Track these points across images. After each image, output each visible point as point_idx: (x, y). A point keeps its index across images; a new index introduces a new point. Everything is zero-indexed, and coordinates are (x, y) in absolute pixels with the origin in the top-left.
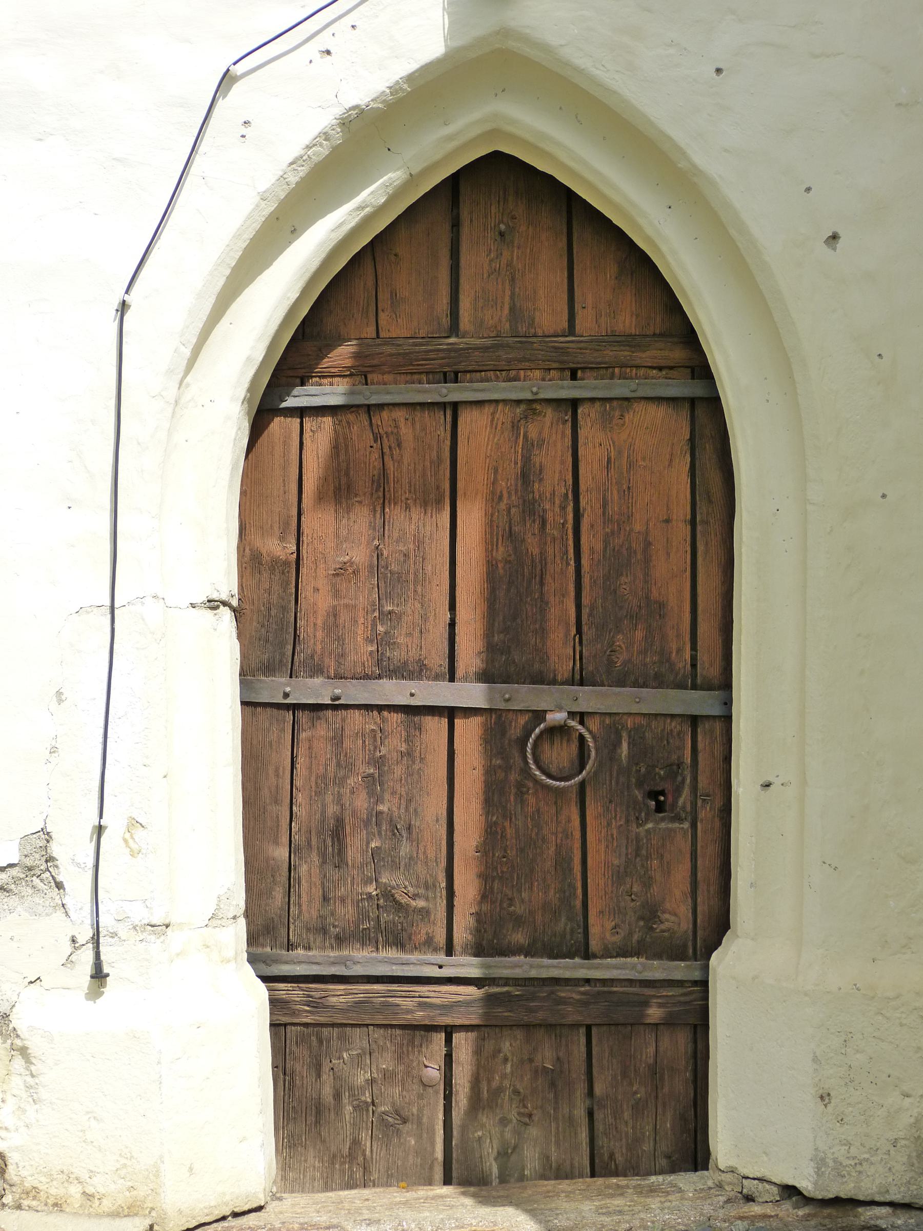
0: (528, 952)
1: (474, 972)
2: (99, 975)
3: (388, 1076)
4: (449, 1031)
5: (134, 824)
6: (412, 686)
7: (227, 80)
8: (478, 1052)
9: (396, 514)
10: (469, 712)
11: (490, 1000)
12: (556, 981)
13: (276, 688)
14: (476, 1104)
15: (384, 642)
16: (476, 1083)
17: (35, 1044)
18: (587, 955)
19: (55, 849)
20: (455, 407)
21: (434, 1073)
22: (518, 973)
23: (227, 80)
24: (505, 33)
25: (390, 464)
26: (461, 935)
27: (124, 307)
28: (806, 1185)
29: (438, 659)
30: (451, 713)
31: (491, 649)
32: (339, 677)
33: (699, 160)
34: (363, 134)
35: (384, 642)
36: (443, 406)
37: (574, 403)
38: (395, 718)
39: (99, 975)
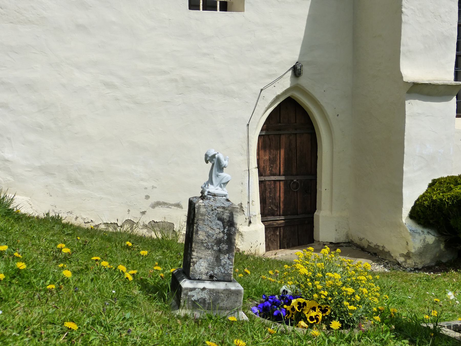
0: (290, 215)
1: (283, 218)
2: (250, 222)
3: (272, 234)
4: (280, 227)
5: (253, 201)
6: (275, 177)
7: (262, 90)
8: (284, 230)
9: (272, 151)
10: (282, 180)
11: (285, 222)
12: (294, 219)
13: (263, 178)
14: (284, 237)
15: (271, 171)
16: (283, 234)
17: (243, 233)
18: (297, 214)
19: (243, 206)
20: (280, 135)
21: (278, 233)
22: (289, 218)
23: (262, 90)
24: (298, 84)
25: (271, 144)
26: (281, 213)
27: (248, 125)
28: (334, 242)
29: (278, 173)
30: (280, 181)
31: (285, 171)
32: (265, 176)
33: (322, 103)
34: (278, 97)
35: (271, 171)
36: (278, 134)
37: (296, 134)
38: (272, 182)
39: (250, 222)
